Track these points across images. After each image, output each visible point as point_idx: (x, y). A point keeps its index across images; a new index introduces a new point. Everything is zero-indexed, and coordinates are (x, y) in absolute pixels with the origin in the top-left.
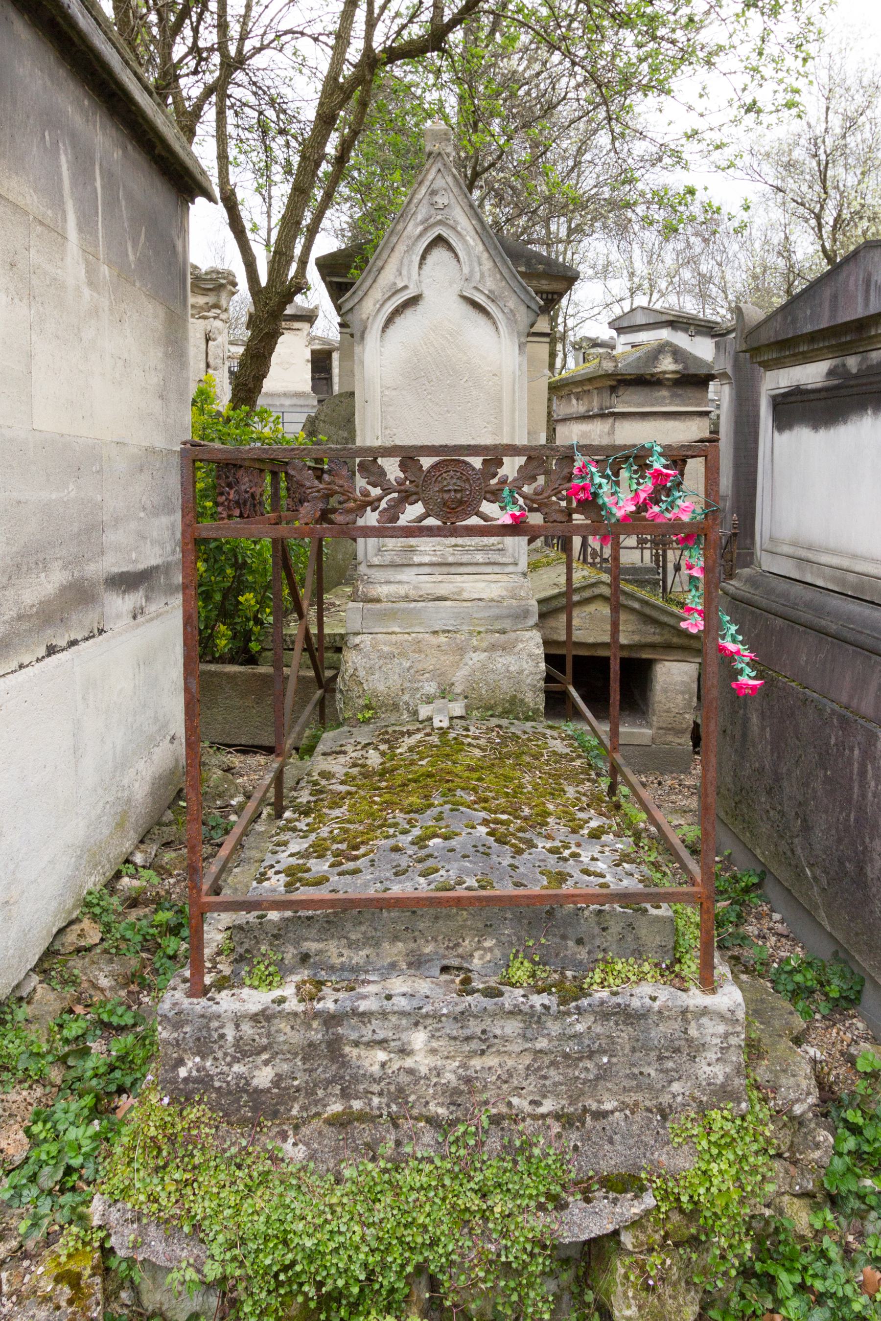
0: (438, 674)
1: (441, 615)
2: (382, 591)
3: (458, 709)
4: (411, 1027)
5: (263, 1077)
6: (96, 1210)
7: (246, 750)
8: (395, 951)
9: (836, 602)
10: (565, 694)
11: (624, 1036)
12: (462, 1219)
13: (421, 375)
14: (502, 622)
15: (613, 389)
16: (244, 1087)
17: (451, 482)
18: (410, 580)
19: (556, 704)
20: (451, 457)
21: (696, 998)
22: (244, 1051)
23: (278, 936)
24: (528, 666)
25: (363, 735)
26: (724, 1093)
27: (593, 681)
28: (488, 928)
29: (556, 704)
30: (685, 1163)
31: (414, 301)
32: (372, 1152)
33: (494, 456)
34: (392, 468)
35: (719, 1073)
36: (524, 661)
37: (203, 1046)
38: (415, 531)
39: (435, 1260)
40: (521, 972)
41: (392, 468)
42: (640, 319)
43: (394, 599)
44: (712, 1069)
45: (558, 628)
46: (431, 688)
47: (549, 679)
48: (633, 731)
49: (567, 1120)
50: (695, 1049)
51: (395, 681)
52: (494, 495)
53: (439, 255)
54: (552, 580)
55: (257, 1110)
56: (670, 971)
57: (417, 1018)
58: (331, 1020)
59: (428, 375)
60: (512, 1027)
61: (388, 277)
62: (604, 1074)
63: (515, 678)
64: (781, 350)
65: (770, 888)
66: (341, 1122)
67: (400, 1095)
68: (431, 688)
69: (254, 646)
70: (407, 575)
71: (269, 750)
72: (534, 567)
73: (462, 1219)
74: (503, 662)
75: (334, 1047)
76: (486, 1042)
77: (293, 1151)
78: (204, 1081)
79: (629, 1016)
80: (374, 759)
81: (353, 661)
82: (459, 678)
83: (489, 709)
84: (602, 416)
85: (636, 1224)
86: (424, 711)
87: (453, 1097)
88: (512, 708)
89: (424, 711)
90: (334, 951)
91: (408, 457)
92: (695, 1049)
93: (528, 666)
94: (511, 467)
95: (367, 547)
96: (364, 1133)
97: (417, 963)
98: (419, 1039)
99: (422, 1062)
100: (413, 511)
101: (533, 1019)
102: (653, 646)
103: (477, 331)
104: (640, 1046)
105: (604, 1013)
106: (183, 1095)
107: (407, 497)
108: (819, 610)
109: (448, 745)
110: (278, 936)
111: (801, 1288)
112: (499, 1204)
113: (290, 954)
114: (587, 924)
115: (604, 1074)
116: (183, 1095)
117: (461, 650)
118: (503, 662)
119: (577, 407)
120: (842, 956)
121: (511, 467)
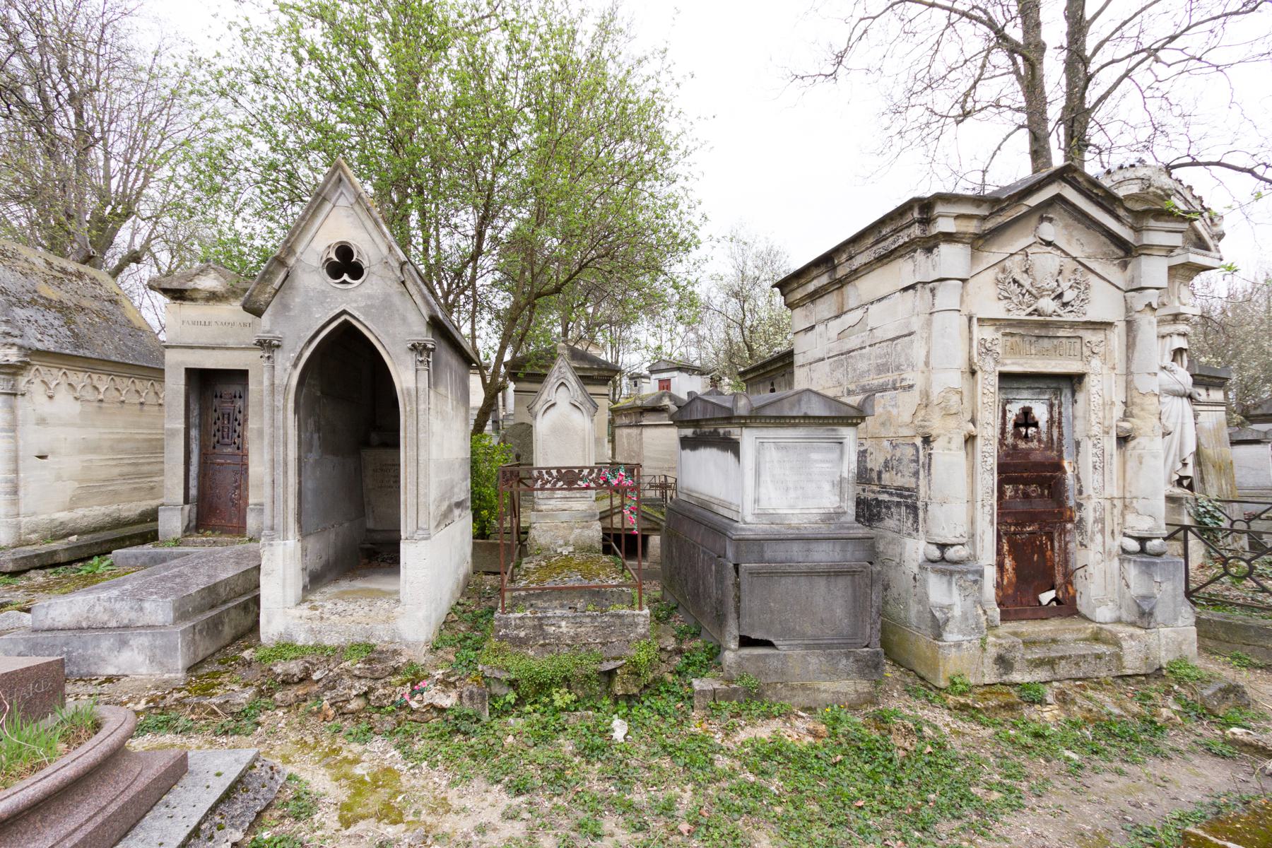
0: (564, 537)
1: (565, 516)
2: (543, 507)
3: (571, 549)
4: (562, 623)
5: (522, 634)
6: (480, 667)
7: (487, 573)
8: (556, 603)
9: (696, 509)
10: (610, 546)
11: (618, 622)
12: (576, 665)
13: (556, 430)
14: (587, 518)
15: (641, 413)
16: (517, 636)
17: (570, 476)
18: (553, 504)
19: (607, 550)
20: (570, 470)
21: (637, 612)
22: (517, 627)
23: (524, 599)
24: (596, 534)
25: (538, 558)
26: (644, 636)
27: (622, 544)
28: (582, 596)
29: (607, 550)
30: (634, 653)
31: (553, 405)
32: (551, 652)
33: (581, 469)
34: (554, 472)
35: (643, 631)
36: (595, 532)
37: (506, 627)
38: (561, 489)
39: (569, 674)
40: (590, 607)
41: (554, 472)
42: (663, 366)
43: (547, 511)
44: (641, 630)
45: (607, 522)
46: (561, 542)
47: (604, 539)
48: (645, 564)
49: (603, 644)
50: (637, 625)
51: (548, 540)
52: (581, 479)
53: (562, 389)
54: (605, 505)
55: (520, 643)
56: (631, 606)
57: (563, 618)
58: (540, 619)
59: (560, 431)
60: (588, 620)
61: (544, 397)
62: (613, 632)
63: (591, 538)
64: (978, 206)
65: (680, 609)
66: (542, 645)
67: (559, 638)
68: (561, 542)
69: (488, 532)
70: (552, 502)
71: (495, 573)
72: (597, 499)
73: (576, 665)
74: (587, 532)
75: (541, 626)
76: (581, 624)
77: (531, 653)
78: (506, 635)
79: (619, 616)
80: (543, 563)
81: (533, 533)
82: (571, 538)
83: (582, 549)
84: (637, 426)
85: (620, 667)
86: (559, 550)
87: (573, 638)
88: (590, 549)
89: (559, 550)
90: (540, 603)
91: (559, 469)
92: (637, 625)
93: (596, 534)
94: (586, 472)
95: (538, 494)
96: (549, 648)
97: (562, 606)
98: (563, 624)
99: (564, 630)
100: (560, 484)
101: (593, 618)
102: (647, 529)
103: (576, 415)
104: (622, 624)
105: (612, 616)
106: (501, 639)
107: (559, 480)
108: (691, 511)
109: (568, 559)
110: (524, 599)
111: (668, 691)
112: (585, 662)
113: (528, 604)
114: (609, 595)
115: (613, 632)
116: (501, 639)
117: (572, 529)
118: (587, 532)
119: (625, 421)
120: (697, 623)
121: (586, 472)
